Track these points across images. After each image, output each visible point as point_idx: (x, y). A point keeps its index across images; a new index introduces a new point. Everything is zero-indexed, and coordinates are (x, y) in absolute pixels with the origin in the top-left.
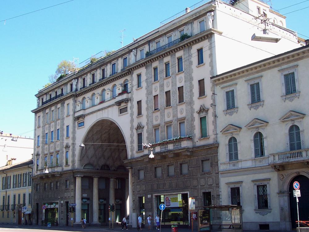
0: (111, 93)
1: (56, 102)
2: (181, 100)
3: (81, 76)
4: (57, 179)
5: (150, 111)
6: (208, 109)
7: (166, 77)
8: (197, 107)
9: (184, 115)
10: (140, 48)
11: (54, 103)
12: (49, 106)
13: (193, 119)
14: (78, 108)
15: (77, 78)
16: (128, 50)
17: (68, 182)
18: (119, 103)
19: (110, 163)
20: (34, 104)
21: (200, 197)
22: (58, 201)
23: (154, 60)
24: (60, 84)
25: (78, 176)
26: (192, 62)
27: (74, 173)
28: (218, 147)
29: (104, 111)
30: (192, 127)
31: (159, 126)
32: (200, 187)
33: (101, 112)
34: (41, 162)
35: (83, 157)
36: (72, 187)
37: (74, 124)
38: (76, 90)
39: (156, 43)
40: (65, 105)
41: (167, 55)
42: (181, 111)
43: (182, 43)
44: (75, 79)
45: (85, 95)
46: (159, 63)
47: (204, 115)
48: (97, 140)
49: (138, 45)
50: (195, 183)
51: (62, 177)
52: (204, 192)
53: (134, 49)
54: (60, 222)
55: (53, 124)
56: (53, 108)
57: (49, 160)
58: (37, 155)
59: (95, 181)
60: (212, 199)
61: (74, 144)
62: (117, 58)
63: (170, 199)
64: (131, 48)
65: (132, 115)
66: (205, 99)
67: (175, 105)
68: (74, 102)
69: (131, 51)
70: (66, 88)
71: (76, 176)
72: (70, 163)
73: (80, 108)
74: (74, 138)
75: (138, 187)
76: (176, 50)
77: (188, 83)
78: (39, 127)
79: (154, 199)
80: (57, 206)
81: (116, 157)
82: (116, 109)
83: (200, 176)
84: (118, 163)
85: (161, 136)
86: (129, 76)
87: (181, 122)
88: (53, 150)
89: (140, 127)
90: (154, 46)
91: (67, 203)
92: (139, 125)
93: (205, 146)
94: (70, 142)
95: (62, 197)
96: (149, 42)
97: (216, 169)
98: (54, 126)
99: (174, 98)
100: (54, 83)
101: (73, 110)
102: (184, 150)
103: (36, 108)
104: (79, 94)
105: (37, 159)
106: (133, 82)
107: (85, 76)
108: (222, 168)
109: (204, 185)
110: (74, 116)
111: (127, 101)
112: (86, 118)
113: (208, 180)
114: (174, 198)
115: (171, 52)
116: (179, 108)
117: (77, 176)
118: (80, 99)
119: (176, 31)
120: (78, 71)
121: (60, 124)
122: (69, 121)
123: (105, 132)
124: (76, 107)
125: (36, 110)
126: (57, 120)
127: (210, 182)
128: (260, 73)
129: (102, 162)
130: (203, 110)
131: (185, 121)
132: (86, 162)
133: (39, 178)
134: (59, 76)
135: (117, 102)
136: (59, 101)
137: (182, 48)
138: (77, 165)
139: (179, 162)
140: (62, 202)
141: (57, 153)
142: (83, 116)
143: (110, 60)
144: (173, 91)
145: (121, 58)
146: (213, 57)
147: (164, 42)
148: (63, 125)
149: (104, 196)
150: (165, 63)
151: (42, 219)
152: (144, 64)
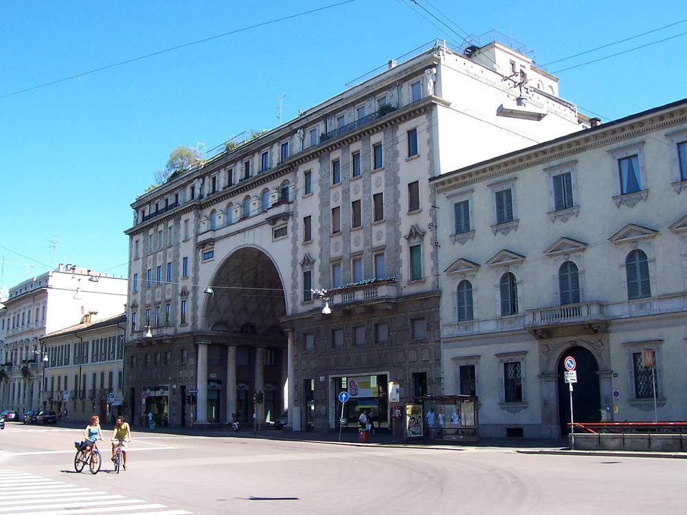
2: (379, 215)
6: (424, 233)
8: (405, 229)
9: (383, 242)
13: (398, 250)
14: (203, 228)
16: (290, 130)
18: (273, 220)
21: (408, 381)
22: (169, 385)
24: (173, 186)
27: (194, 338)
33: (242, 235)
35: (212, 311)
37: (196, 254)
40: (182, 222)
41: (336, 148)
44: (198, 177)
46: (343, 153)
50: (400, 357)
53: (300, 128)
56: (161, 227)
59: (232, 351)
61: (195, 289)
62: (271, 144)
63: (356, 384)
65: (295, 240)
67: (368, 225)
69: (295, 131)
72: (189, 320)
82: (267, 230)
85: (344, 277)
87: (379, 253)
89: (308, 261)
90: (333, 125)
91: (183, 388)
96: (325, 118)
97: (436, 333)
99: (367, 213)
104: (206, 203)
108: (445, 332)
110: (196, 240)
111: (286, 216)
116: (375, 229)
118: (207, 212)
122: (187, 250)
126: (167, 248)
129: (243, 320)
130: (415, 233)
138: (200, 324)
140: (175, 386)
142: (211, 242)
147: (351, 116)
148: (178, 255)
149: (245, 377)
150: (352, 153)
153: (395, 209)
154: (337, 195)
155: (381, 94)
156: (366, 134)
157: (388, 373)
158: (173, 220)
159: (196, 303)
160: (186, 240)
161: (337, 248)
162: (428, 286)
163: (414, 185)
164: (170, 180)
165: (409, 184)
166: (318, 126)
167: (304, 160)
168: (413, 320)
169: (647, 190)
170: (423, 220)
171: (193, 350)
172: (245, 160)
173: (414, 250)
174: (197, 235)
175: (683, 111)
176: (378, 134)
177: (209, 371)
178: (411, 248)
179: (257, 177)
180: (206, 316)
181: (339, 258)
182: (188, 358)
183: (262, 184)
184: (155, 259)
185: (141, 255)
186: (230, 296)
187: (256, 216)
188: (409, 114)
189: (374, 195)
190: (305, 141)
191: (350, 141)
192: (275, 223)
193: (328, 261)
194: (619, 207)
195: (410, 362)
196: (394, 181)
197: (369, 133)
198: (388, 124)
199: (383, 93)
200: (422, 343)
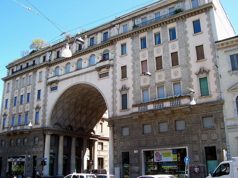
0: (88, 62)
1: (28, 71)
3: (55, 50)
4: (25, 136)
5: (137, 75)
7: (141, 49)
10: (124, 23)
11: (25, 72)
12: (20, 74)
14: (50, 75)
15: (51, 51)
16: (112, 25)
17: (37, 139)
18: (99, 69)
19: (73, 124)
20: (5, 73)
21: (202, 152)
22: (25, 156)
24: (33, 56)
25: (49, 133)
26: (187, 31)
27: (44, 131)
28: (223, 104)
29: (80, 76)
32: (201, 142)
33: (77, 77)
34: (8, 121)
35: (53, 117)
36: (41, 143)
37: (46, 88)
38: (50, 60)
39: (141, 19)
40: (38, 73)
42: (176, 74)
43: (177, 15)
44: (49, 51)
45: (81, 56)
46: (148, 34)
47: (204, 76)
48: (66, 103)
49: (122, 21)
50: (195, 138)
51: (31, 134)
53: (117, 24)
54: (26, 174)
55: (24, 89)
56: (24, 76)
57: (17, 119)
59: (61, 139)
60: (218, 154)
61: (45, 105)
62: (97, 33)
63: (161, 154)
64: (113, 24)
65: (114, 79)
66: (204, 62)
67: (168, 68)
68: (47, 71)
69: (114, 26)
70: (38, 60)
71: (46, 133)
72: (40, 122)
73: (53, 75)
74: (45, 101)
75: (122, 143)
76: (140, 32)
77: (183, 50)
78: (8, 92)
79: (142, 155)
80: (23, 160)
81: (78, 120)
82: (96, 74)
83: (200, 132)
84: (79, 125)
85: (150, 95)
86: (112, 46)
87: (176, 82)
88: (15, 112)
89: (124, 88)
90: (139, 21)
91: (35, 157)
92: (124, 87)
93: (209, 104)
94: (41, 103)
95: (29, 152)
96: (133, 19)
97: (222, 124)
98: (24, 91)
99: (25, 99)
101: (45, 77)
102: (186, 107)
103: (6, 76)
104: (53, 64)
105: (4, 119)
106: (116, 50)
108: (228, 123)
109: (217, 139)
110: (47, 82)
111: (108, 67)
112: (60, 83)
113: (212, 135)
114: (166, 153)
115: (162, 24)
116: (20, 107)
117: (48, 134)
118: (53, 68)
119: (151, 13)
120: (52, 45)
121: (31, 89)
122: (41, 86)
123: (75, 97)
124: (48, 74)
125: (7, 78)
126: (28, 86)
127: (214, 137)
128: (235, 47)
129: (67, 123)
130: (38, 108)
131: (181, 82)
132: (55, 122)
133: (6, 135)
134: (32, 50)
135: (99, 67)
136: (32, 69)
138: (47, 124)
139: (173, 119)
140: (29, 156)
141: (27, 113)
142: (57, 82)
143: (89, 34)
144: (165, 56)
145: (100, 33)
146: (212, 27)
147: (151, 17)
148: (35, 89)
149: (67, 153)
150: (154, 34)
151: (5, 170)
152: (130, 35)
153: (187, 59)
154: (159, 50)
157: (142, 150)
158: (32, 72)
159: (45, 113)
160: (40, 81)
161: (145, 81)
162: (214, 97)
163: (124, 67)
165: (122, 67)
166: (129, 23)
167: (39, 68)
168: (143, 125)
170: (41, 103)
172: (57, 50)
174: (47, 79)
175: (237, 41)
177: (51, 148)
178: (36, 112)
180: (51, 119)
181: (147, 86)
182: (39, 141)
183: (55, 64)
184: (19, 91)
185: (11, 90)
186: (63, 110)
187: (52, 77)
188: (41, 66)
189: (156, 58)
190: (119, 30)
192: (100, 71)
193: (140, 88)
194: (231, 76)
195: (202, 141)
198: (180, 18)
200: (210, 130)
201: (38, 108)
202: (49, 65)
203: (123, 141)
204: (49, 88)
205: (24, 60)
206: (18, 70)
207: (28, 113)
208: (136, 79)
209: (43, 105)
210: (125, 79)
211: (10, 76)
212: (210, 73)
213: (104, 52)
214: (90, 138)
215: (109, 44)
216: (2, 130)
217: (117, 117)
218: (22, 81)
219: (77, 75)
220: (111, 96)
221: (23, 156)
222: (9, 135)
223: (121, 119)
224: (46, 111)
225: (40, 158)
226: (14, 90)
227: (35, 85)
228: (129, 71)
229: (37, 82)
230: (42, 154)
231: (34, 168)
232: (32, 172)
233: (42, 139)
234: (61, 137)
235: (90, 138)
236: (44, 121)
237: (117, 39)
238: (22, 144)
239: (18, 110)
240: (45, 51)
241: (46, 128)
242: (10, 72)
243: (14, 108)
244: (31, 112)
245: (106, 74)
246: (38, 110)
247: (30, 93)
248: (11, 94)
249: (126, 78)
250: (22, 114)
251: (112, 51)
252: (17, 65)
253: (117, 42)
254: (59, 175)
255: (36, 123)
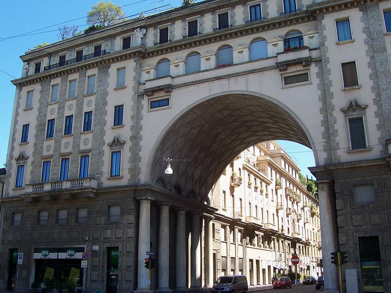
2: (87, 127)
6: (124, 143)
8: (109, 138)
9: (89, 146)
13: (101, 153)
14: (145, 77)
17: (115, 211)
18: (282, 66)
20: (18, 70)
23: (56, 76)
27: (134, 194)
29: (232, 80)
30: (100, 163)
31: (90, 152)
33: (223, 81)
38: (143, 45)
41: (57, 77)
44: (141, 28)
47: (356, 115)
52: (109, 247)
54: (88, 286)
58: (18, 160)
61: (136, 138)
62: (173, 21)
71: (144, 197)
74: (137, 129)
78: (28, 108)
87: (85, 155)
89: (22, 157)
94: (125, 133)
99: (78, 125)
100: (75, 38)
107: (198, 16)
109: (121, 238)
111: (307, 62)
115: (80, 69)
116: (64, 141)
117: (147, 199)
118: (154, 61)
119: (72, 50)
122: (126, 98)
130: (117, 143)
137: (60, 74)
140: (96, 248)
142: (168, 89)
148: (105, 104)
155: (98, 43)
156: (66, 73)
159: (137, 154)
160: (120, 87)
164: (86, 32)
166: (43, 60)
169: (322, 126)
170: (125, 133)
171: (132, 206)
173: (116, 155)
176: (57, 79)
179: (180, 41)
185: (36, 104)
191: (52, 77)
196: (102, 103)
197: (50, 77)
199: (100, 42)
201: (117, 143)
202: (142, 55)
203: (360, 214)
204: (145, 102)
205: (74, 44)
206: (44, 69)
207: (90, 154)
208: (381, 88)
209: (131, 137)
210: (355, 87)
211: (31, 76)
212: (367, 110)
213: (286, 35)
214: (205, 214)
215: (303, 18)
216: (14, 190)
217: (340, 163)
218: (68, 87)
219: (225, 76)
220: (320, 122)
221: (77, 246)
222: (36, 200)
223: (352, 168)
224: (140, 150)
225: (128, 252)
226: (43, 106)
227: (105, 94)
228: (363, 73)
229: (110, 89)
230: (133, 244)
231: (108, 273)
232: (105, 283)
233: (133, 211)
234: (165, 207)
235: (205, 214)
236: (135, 171)
237: (327, 9)
238: (72, 222)
239: (76, 145)
240: (129, 27)
241: (342, 164)
242: (31, 68)
243: (46, 144)
244: (98, 152)
245: (303, 78)
246: (118, 147)
247: (92, 112)
248: (37, 113)
249: (357, 87)
250: (70, 157)
251: (309, 33)
252: (50, 55)
253: (23, 88)
254: (163, 288)
255: (114, 174)
